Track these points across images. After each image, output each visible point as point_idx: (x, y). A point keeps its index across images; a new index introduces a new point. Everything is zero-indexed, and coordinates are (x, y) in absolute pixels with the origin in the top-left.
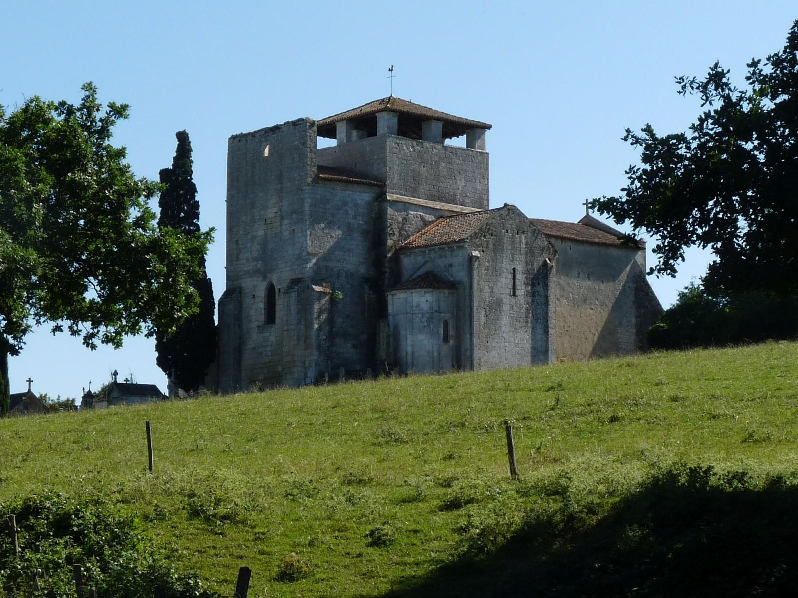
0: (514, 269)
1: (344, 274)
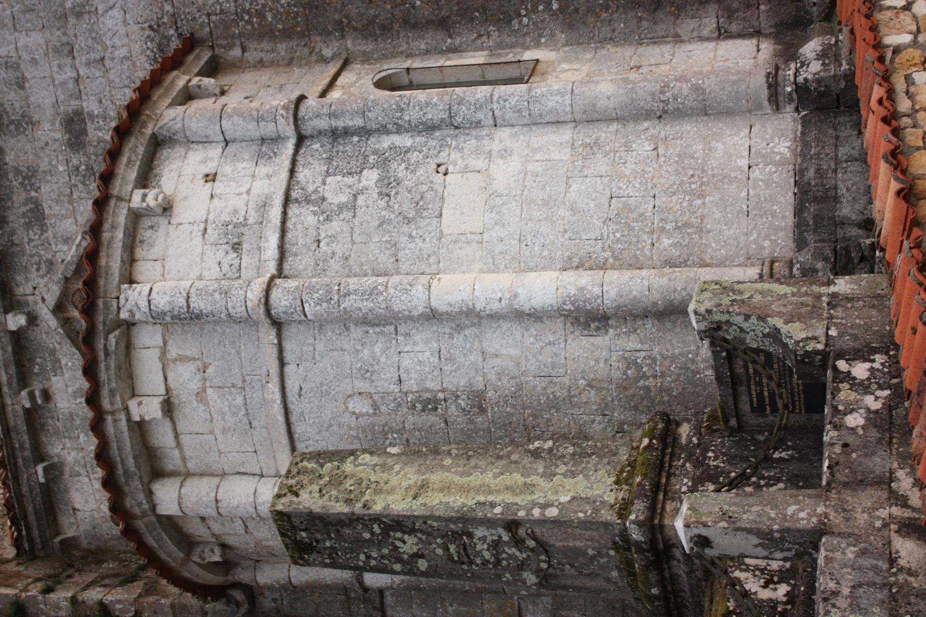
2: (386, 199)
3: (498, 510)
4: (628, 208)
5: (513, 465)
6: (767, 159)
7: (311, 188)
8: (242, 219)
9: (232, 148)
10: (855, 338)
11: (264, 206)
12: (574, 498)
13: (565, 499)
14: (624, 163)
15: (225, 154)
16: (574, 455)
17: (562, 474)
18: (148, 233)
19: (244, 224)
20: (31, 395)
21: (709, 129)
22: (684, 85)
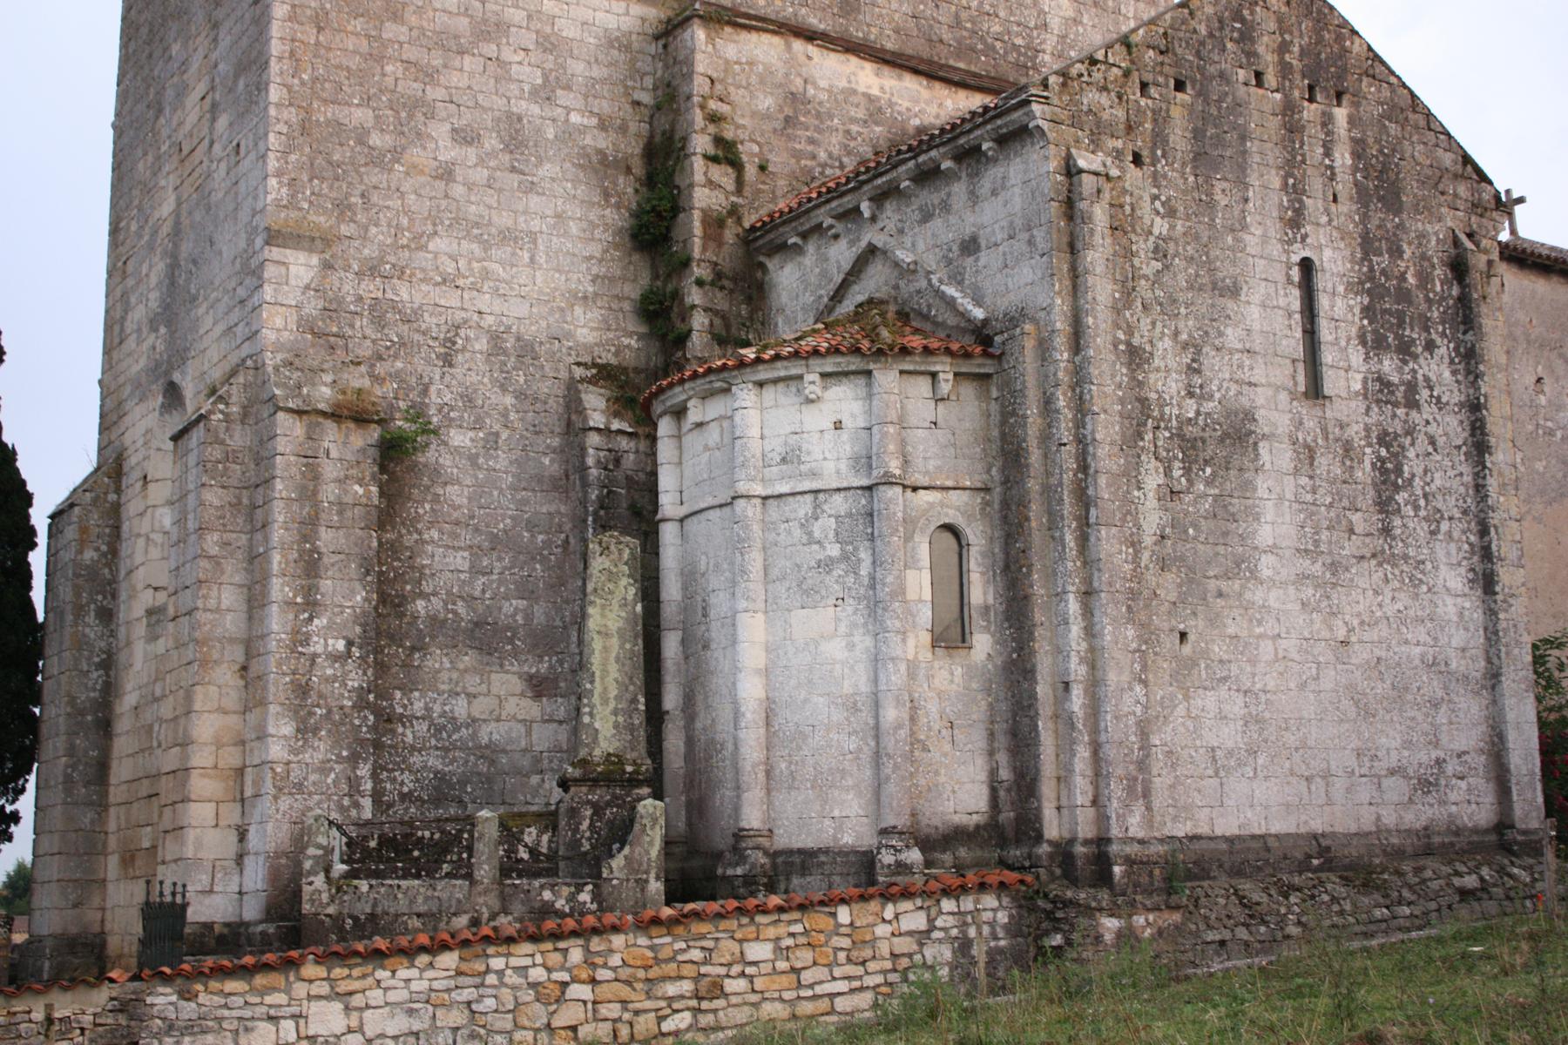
0: (1306, 266)
1: (482, 344)
3: (588, 686)
4: (804, 737)
6: (839, 829)
7: (825, 507)
9: (864, 434)
10: (610, 894)
11: (814, 474)
13: (597, 725)
18: (794, 389)
19: (800, 462)
20: (831, 227)
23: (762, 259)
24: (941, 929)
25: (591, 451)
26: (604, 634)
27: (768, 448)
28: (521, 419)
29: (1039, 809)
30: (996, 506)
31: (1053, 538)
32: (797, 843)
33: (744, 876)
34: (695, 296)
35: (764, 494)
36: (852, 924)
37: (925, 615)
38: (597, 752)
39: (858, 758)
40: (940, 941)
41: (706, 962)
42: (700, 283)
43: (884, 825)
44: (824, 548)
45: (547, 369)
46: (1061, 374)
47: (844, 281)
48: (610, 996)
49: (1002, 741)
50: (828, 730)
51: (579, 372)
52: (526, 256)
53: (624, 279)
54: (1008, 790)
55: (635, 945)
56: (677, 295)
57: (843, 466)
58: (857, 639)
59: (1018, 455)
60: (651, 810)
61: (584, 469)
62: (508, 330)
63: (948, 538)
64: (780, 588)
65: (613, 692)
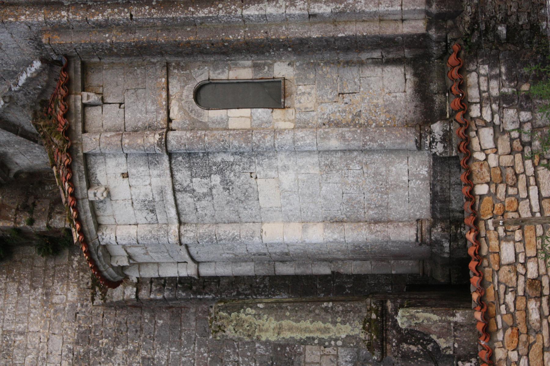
2: (228, 191)
4: (351, 198)
5: (317, 317)
6: (417, 177)
7: (185, 185)
8: (151, 199)
9: (130, 158)
10: (464, 349)
11: (162, 192)
12: (347, 336)
13: (343, 336)
14: (347, 177)
15: (128, 161)
16: (342, 311)
17: (340, 322)
19: (154, 200)
21: (387, 159)
22: (375, 144)
23: (12, 176)
24: (493, 118)
25: (152, 296)
26: (280, 330)
27: (144, 221)
28: (133, 340)
29: (403, 36)
30: (180, 59)
31: (201, 24)
32: (428, 204)
33: (450, 242)
34: (41, 225)
35: (177, 225)
36: (488, 183)
37: (261, 113)
38: (362, 336)
39: (366, 164)
40: (501, 118)
41: (515, 291)
42: (31, 222)
43: (415, 148)
44: (215, 186)
45: (97, 322)
46: (79, 18)
47: (21, 135)
48: (539, 360)
49: (352, 56)
50: (349, 184)
51: (98, 300)
52: (19, 338)
53: (32, 266)
54: (389, 53)
55: (503, 342)
56: (41, 235)
57: (155, 172)
58: (279, 164)
59: (141, 47)
60: (405, 319)
61: (164, 299)
62: (71, 351)
63: (203, 94)
64: (244, 214)
65: (320, 324)
